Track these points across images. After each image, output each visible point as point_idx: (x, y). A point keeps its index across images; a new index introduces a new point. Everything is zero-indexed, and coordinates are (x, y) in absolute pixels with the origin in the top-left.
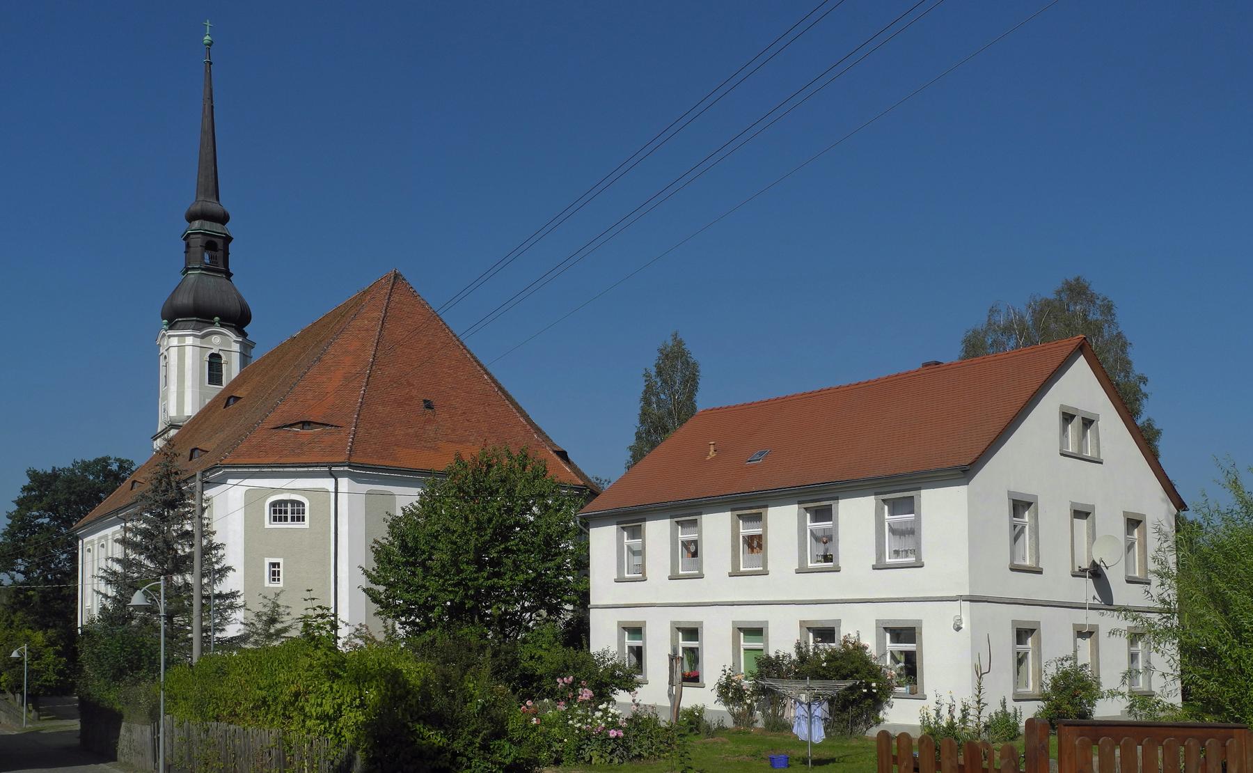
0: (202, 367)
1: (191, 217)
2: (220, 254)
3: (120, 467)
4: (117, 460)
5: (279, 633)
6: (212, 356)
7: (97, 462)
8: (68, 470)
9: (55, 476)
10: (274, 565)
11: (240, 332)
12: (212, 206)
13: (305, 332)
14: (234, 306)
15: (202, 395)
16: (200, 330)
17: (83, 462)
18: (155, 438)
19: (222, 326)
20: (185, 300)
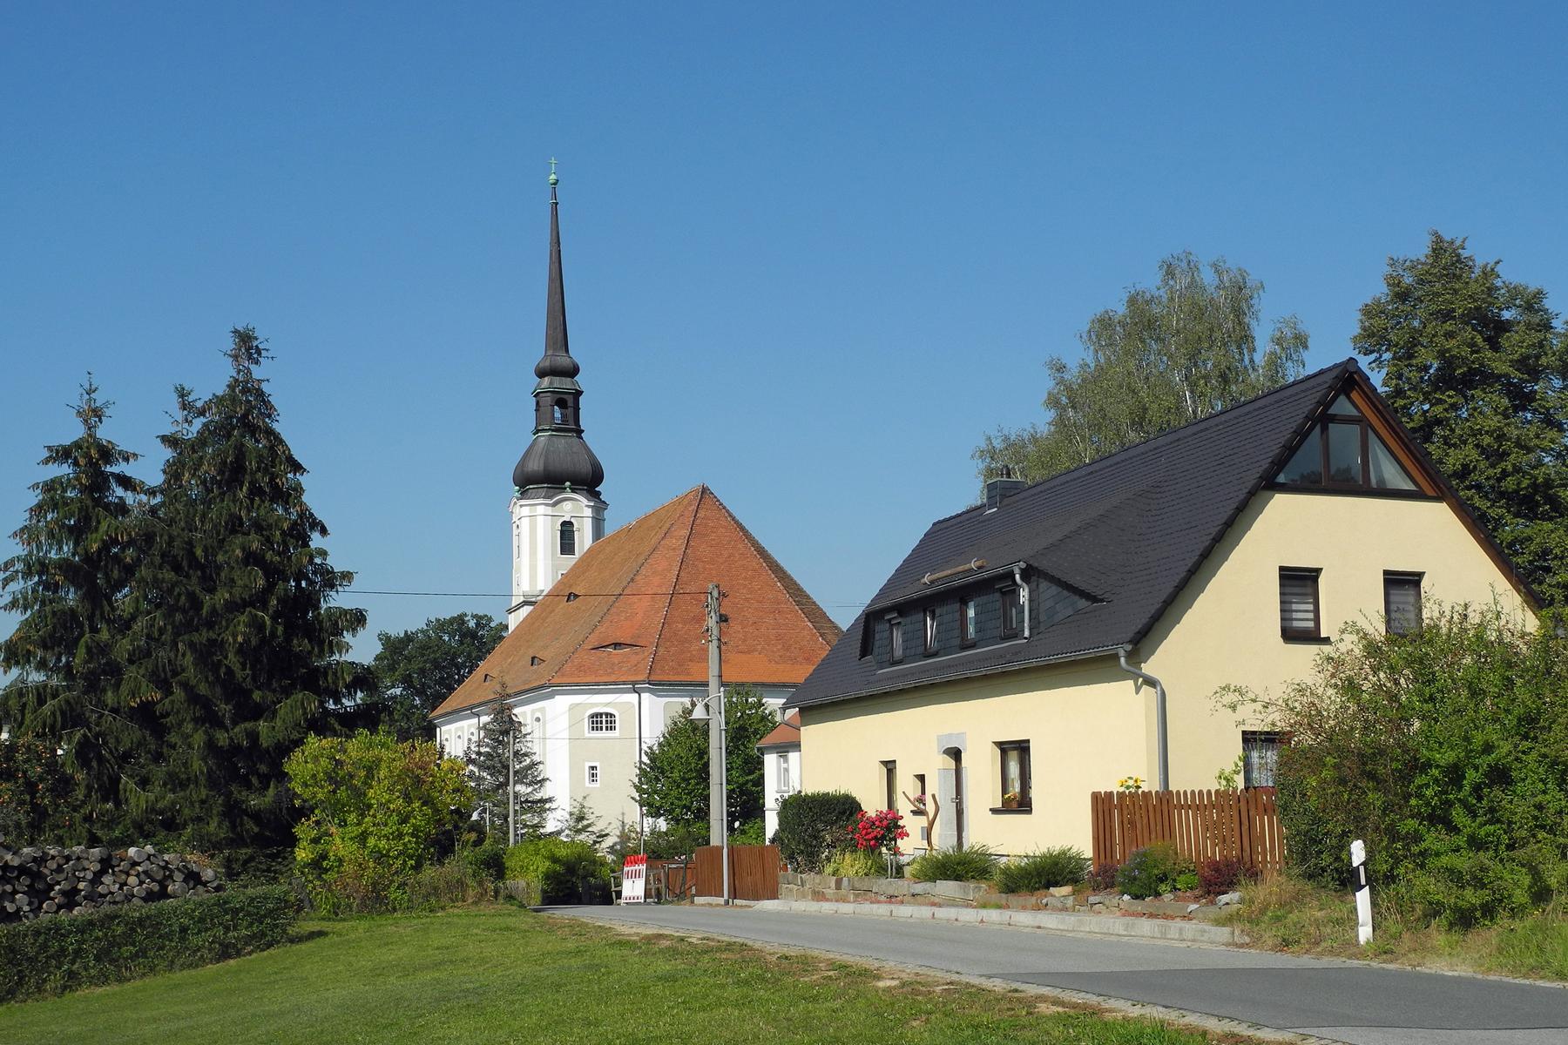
0: (553, 537)
1: (541, 374)
2: (570, 411)
3: (478, 624)
4: (474, 616)
5: (584, 829)
6: (564, 524)
7: (452, 621)
8: (422, 631)
9: (409, 638)
10: (593, 768)
11: (594, 495)
12: (562, 361)
13: (641, 522)
14: (585, 468)
15: (555, 568)
16: (550, 497)
17: (438, 620)
18: (510, 611)
19: (573, 491)
20: (535, 465)
